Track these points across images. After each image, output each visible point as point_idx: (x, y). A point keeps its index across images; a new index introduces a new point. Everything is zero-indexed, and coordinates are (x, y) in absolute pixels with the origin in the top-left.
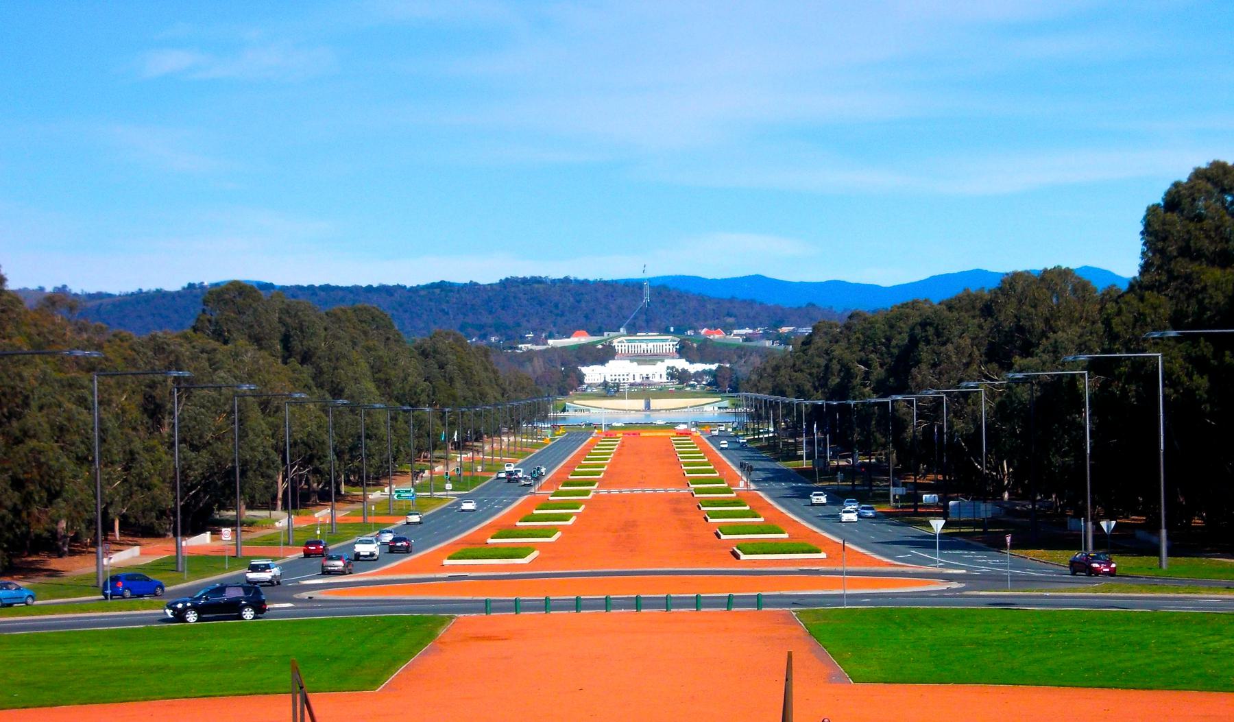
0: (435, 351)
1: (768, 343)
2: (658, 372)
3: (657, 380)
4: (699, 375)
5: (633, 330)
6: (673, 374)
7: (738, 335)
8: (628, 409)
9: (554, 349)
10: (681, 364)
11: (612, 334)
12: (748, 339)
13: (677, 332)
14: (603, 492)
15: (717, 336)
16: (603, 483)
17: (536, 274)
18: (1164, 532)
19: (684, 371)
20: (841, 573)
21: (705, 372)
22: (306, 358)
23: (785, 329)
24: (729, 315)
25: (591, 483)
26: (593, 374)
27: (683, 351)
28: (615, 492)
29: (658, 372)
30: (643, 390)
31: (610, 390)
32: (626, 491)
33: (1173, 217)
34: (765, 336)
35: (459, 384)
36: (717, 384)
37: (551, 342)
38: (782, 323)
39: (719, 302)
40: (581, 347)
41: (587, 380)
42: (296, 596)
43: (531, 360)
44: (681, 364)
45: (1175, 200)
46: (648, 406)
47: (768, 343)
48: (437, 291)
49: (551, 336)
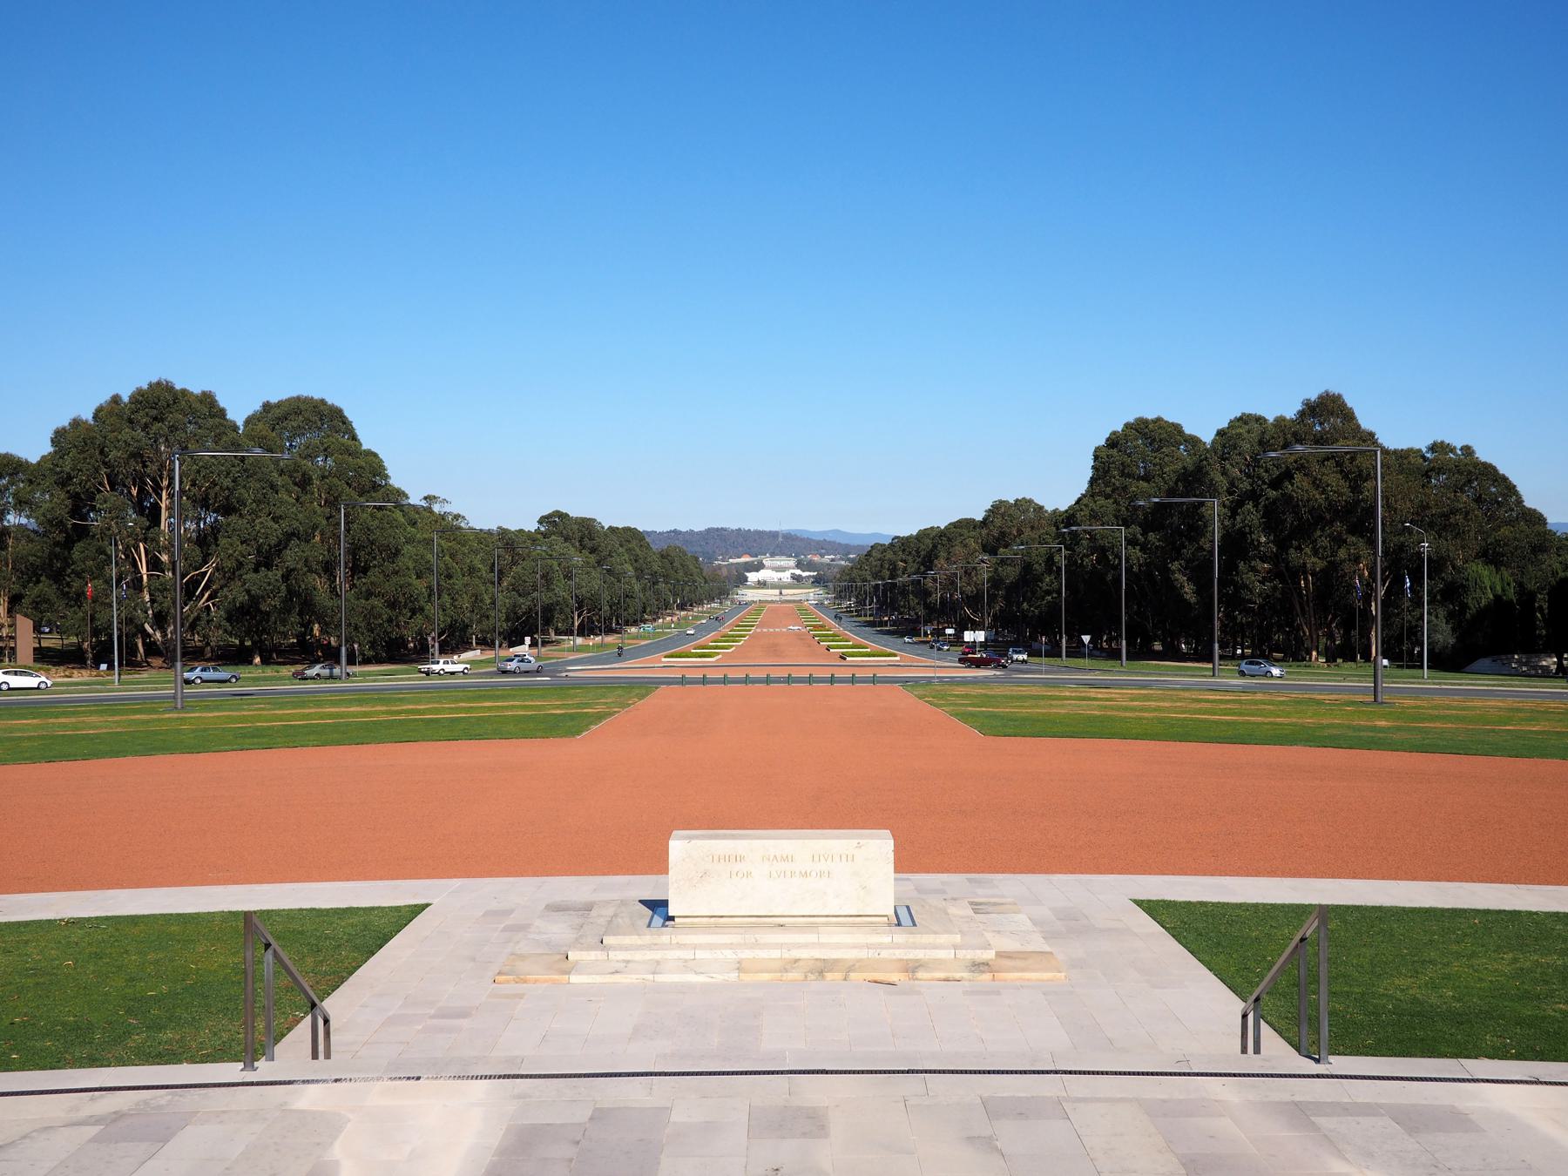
0: (668, 555)
1: (843, 563)
2: (786, 576)
3: (785, 580)
4: (809, 577)
5: (773, 555)
6: (794, 577)
7: (827, 558)
8: (770, 594)
9: (732, 564)
10: (798, 572)
11: (763, 557)
12: (833, 560)
13: (795, 557)
14: (759, 630)
15: (816, 559)
16: (758, 626)
17: (724, 526)
18: (1124, 642)
19: (800, 576)
20: (911, 666)
21: (810, 576)
22: (593, 551)
23: (851, 556)
24: (822, 549)
25: (753, 626)
26: (753, 577)
27: (799, 565)
28: (765, 630)
29: (786, 576)
30: (780, 586)
31: (762, 585)
32: (771, 630)
33: (1114, 452)
34: (841, 559)
35: (681, 573)
36: (818, 581)
37: (731, 560)
38: (849, 553)
39: (818, 542)
40: (746, 563)
41: (749, 580)
42: (558, 675)
43: (720, 569)
44: (798, 572)
45: (1113, 442)
46: (781, 593)
47: (843, 563)
48: (673, 534)
49: (731, 558)
